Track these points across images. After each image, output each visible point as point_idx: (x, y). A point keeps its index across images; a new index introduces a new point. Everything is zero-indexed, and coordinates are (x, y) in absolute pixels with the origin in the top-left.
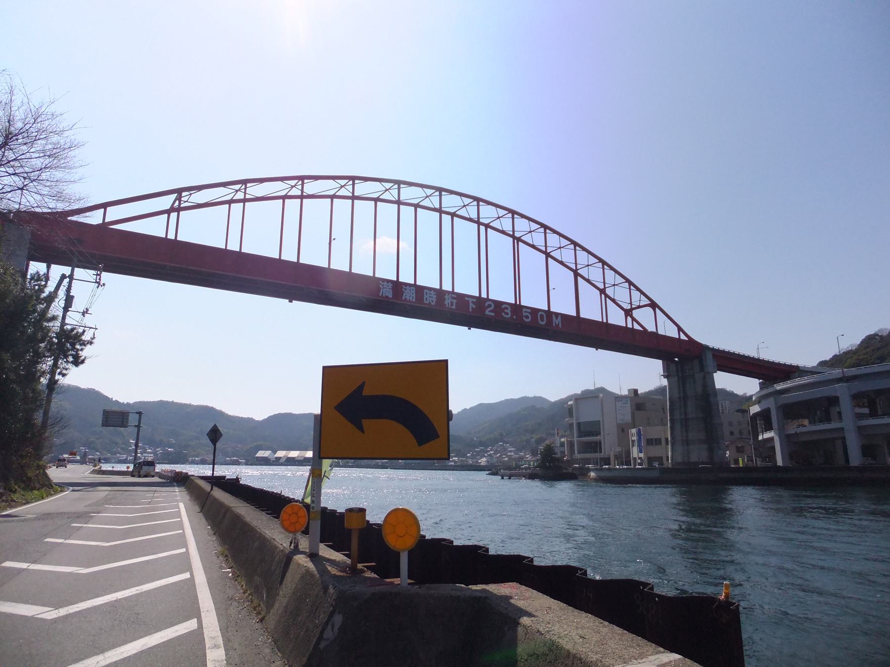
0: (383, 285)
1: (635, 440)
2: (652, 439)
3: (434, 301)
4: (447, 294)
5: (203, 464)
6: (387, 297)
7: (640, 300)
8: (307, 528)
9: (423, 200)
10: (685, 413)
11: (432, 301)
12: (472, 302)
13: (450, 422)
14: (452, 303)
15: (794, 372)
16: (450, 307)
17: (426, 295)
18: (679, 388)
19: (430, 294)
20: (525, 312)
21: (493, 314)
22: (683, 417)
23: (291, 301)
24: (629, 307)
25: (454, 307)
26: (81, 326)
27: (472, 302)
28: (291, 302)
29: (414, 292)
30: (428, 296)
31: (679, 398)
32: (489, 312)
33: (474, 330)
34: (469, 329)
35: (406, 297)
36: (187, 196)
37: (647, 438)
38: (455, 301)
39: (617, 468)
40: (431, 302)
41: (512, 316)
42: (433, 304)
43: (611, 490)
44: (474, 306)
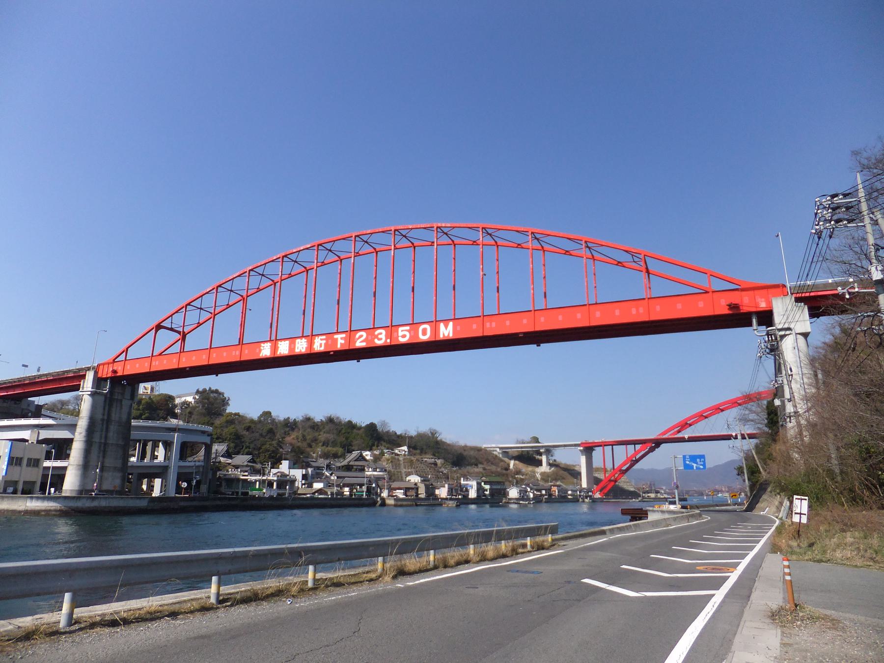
2: (32, 459)
6: (266, 355)
10: (106, 437)
11: (303, 348)
12: (341, 339)
18: (104, 409)
20: (402, 331)
21: (364, 344)
22: (103, 441)
23: (538, 345)
26: (801, 366)
27: (341, 339)
28: (539, 346)
31: (103, 420)
32: (361, 342)
33: (544, 346)
35: (281, 351)
39: (459, 498)
42: (451, 335)
44: (343, 342)
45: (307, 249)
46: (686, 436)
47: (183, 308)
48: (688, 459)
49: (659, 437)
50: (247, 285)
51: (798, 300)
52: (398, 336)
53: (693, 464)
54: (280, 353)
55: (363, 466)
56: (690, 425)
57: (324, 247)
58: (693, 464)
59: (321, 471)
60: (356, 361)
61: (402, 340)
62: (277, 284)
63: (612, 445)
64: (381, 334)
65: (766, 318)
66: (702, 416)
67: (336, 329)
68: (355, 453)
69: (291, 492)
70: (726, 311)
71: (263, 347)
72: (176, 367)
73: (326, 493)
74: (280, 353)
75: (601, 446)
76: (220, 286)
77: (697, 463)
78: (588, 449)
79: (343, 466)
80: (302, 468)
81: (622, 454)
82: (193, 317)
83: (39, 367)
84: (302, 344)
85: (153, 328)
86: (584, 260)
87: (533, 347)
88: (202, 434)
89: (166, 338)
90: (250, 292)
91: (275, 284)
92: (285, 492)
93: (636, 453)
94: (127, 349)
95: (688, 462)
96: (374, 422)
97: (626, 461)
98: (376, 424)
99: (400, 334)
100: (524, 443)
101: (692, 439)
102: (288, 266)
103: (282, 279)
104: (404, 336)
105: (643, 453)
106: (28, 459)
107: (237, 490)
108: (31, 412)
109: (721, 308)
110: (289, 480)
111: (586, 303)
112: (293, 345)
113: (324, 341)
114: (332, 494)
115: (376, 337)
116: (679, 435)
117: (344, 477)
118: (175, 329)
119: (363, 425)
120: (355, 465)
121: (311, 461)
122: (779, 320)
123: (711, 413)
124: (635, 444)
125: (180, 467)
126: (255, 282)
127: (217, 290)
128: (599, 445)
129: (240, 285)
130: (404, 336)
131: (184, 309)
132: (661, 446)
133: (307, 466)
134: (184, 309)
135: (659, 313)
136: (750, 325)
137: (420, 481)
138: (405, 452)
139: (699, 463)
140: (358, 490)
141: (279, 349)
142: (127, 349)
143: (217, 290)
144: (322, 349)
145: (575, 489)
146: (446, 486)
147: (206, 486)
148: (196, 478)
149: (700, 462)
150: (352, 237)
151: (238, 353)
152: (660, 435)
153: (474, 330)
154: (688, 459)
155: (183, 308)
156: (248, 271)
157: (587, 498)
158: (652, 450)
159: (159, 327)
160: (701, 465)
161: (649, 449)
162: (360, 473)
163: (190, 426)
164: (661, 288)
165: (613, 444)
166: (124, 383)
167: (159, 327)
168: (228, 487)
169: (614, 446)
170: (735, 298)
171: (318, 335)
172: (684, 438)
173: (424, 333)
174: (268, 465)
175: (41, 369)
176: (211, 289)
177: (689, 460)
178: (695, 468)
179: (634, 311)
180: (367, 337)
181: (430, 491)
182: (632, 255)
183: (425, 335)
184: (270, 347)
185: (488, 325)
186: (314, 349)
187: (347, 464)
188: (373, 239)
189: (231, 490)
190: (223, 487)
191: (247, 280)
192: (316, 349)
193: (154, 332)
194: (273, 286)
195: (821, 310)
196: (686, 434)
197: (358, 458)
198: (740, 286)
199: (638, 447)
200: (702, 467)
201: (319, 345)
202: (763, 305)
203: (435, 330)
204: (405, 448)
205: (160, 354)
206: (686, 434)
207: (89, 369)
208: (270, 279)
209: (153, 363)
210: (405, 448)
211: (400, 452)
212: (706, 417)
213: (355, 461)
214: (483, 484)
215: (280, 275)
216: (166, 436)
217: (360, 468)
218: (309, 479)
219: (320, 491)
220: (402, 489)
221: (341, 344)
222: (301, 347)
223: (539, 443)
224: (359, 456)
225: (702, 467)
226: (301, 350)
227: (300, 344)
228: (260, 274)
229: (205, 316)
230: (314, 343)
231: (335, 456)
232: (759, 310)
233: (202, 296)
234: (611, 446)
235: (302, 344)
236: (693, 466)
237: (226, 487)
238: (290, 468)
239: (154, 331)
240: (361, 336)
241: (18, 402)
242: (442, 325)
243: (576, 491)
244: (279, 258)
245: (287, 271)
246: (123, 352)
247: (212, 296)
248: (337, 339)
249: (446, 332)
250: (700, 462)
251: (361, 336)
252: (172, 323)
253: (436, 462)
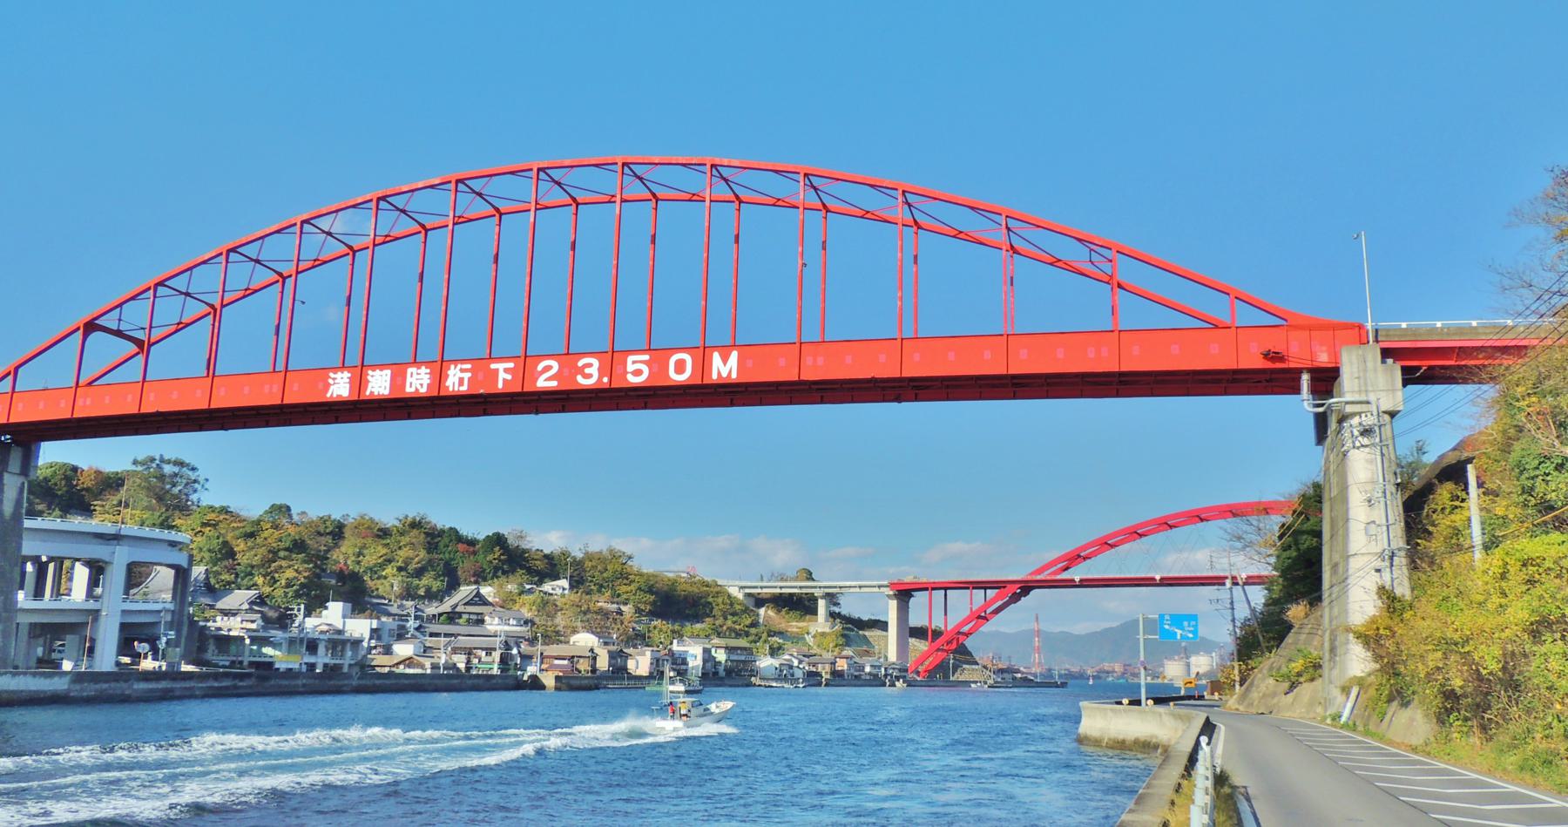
1: (432, 664)
5: (174, 542)
8: (1063, 718)
9: (788, 172)
11: (422, 385)
12: (506, 370)
14: (461, 381)
15: (1290, 596)
17: (412, 376)
19: (418, 374)
20: (634, 362)
21: (553, 384)
27: (506, 370)
32: (546, 380)
35: (373, 390)
42: (734, 376)
44: (509, 377)
45: (432, 187)
46: (1077, 579)
47: (149, 289)
48: (1167, 620)
49: (1030, 578)
50: (296, 252)
51: (1386, 353)
52: (626, 373)
53: (1176, 630)
54: (372, 393)
55: (482, 614)
56: (1085, 558)
57: (467, 186)
58: (1176, 630)
59: (404, 623)
61: (634, 380)
62: (287, 280)
63: (946, 589)
64: (590, 365)
65: (1326, 381)
66: (1105, 544)
67: (488, 351)
68: (465, 591)
69: (352, 662)
70: (1259, 363)
71: (334, 379)
72: (133, 410)
73: (422, 666)
74: (372, 393)
75: (926, 589)
76: (234, 250)
77: (1182, 629)
78: (904, 594)
79: (440, 615)
80: (371, 617)
81: (962, 605)
82: (169, 309)
84: (419, 377)
85: (78, 329)
86: (1004, 252)
88: (170, 548)
89: (103, 349)
90: (228, 297)
91: (284, 279)
92: (341, 662)
93: (988, 604)
94: (16, 369)
96: (501, 532)
97: (969, 617)
98: (506, 533)
99: (630, 368)
100: (786, 580)
101: (1086, 583)
102: (389, 221)
103: (376, 243)
104: (638, 373)
105: (999, 603)
107: (240, 659)
109: (1252, 359)
110: (349, 640)
111: (1002, 333)
112: (400, 379)
113: (469, 375)
114: (435, 667)
115: (581, 371)
116: (1065, 576)
117: (455, 635)
118: (127, 333)
119: (481, 537)
122: (1349, 387)
123: (1122, 539)
124: (985, 588)
125: (124, 612)
126: (241, 273)
127: (155, 292)
128: (923, 588)
129: (207, 282)
130: (637, 372)
131: (151, 291)
132: (1032, 593)
133: (378, 611)
134: (151, 291)
135: (1137, 360)
136: (1296, 390)
137: (596, 645)
138: (564, 589)
139: (1187, 629)
140: (483, 660)
141: (370, 385)
142: (16, 369)
143: (155, 292)
144: (464, 388)
145: (878, 664)
146: (648, 654)
147: (178, 649)
148: (166, 635)
149: (1189, 626)
150: (531, 170)
151: (277, 389)
152: (1032, 574)
153: (783, 371)
154: (1167, 620)
155: (149, 289)
156: (224, 254)
157: (898, 681)
158: (1015, 598)
159: (91, 327)
160: (1190, 632)
161: (1010, 598)
162: (477, 628)
164: (1136, 315)
165: (946, 588)
167: (91, 327)
168: (220, 652)
169: (948, 591)
170: (1275, 343)
171: (456, 362)
172: (1073, 580)
173: (680, 367)
174: (299, 610)
176: (214, 254)
177: (1169, 622)
178: (1179, 637)
179: (1091, 353)
180: (560, 371)
181: (619, 658)
183: (680, 371)
184: (348, 380)
185: (808, 361)
186: (448, 387)
187: (449, 610)
188: (570, 178)
189: (229, 658)
190: (210, 651)
191: (297, 242)
192: (451, 389)
193: (81, 337)
194: (279, 285)
195: (1418, 374)
196: (1076, 574)
197: (472, 599)
198: (1286, 320)
199: (991, 593)
200: (1191, 635)
201: (457, 380)
202: (1323, 359)
203: (703, 364)
204: (564, 583)
205: (90, 384)
206: (1076, 574)
208: (416, 221)
209: (79, 402)
210: (564, 583)
211: (553, 589)
212: (1112, 546)
213: (465, 604)
214: (713, 651)
215: (372, 236)
216: (98, 551)
217: (474, 617)
218: (385, 636)
219: (408, 662)
220: (565, 659)
221: (505, 381)
222: (418, 382)
223: (813, 580)
224: (475, 596)
225: (1191, 635)
226: (417, 389)
227: (415, 376)
228: (181, 293)
229: (194, 309)
230: (447, 376)
231: (431, 596)
232: (1316, 364)
233: (190, 269)
234: (943, 591)
235: (419, 377)
236: (1176, 633)
237: (216, 651)
238: (344, 617)
239: (79, 334)
240: (548, 368)
242: (716, 357)
243: (879, 667)
244: (371, 200)
245: (309, 254)
246: (9, 374)
247: (291, 240)
248: (497, 371)
249: (725, 368)
250: (1189, 626)
251: (548, 368)
252: (120, 320)
253: (620, 609)
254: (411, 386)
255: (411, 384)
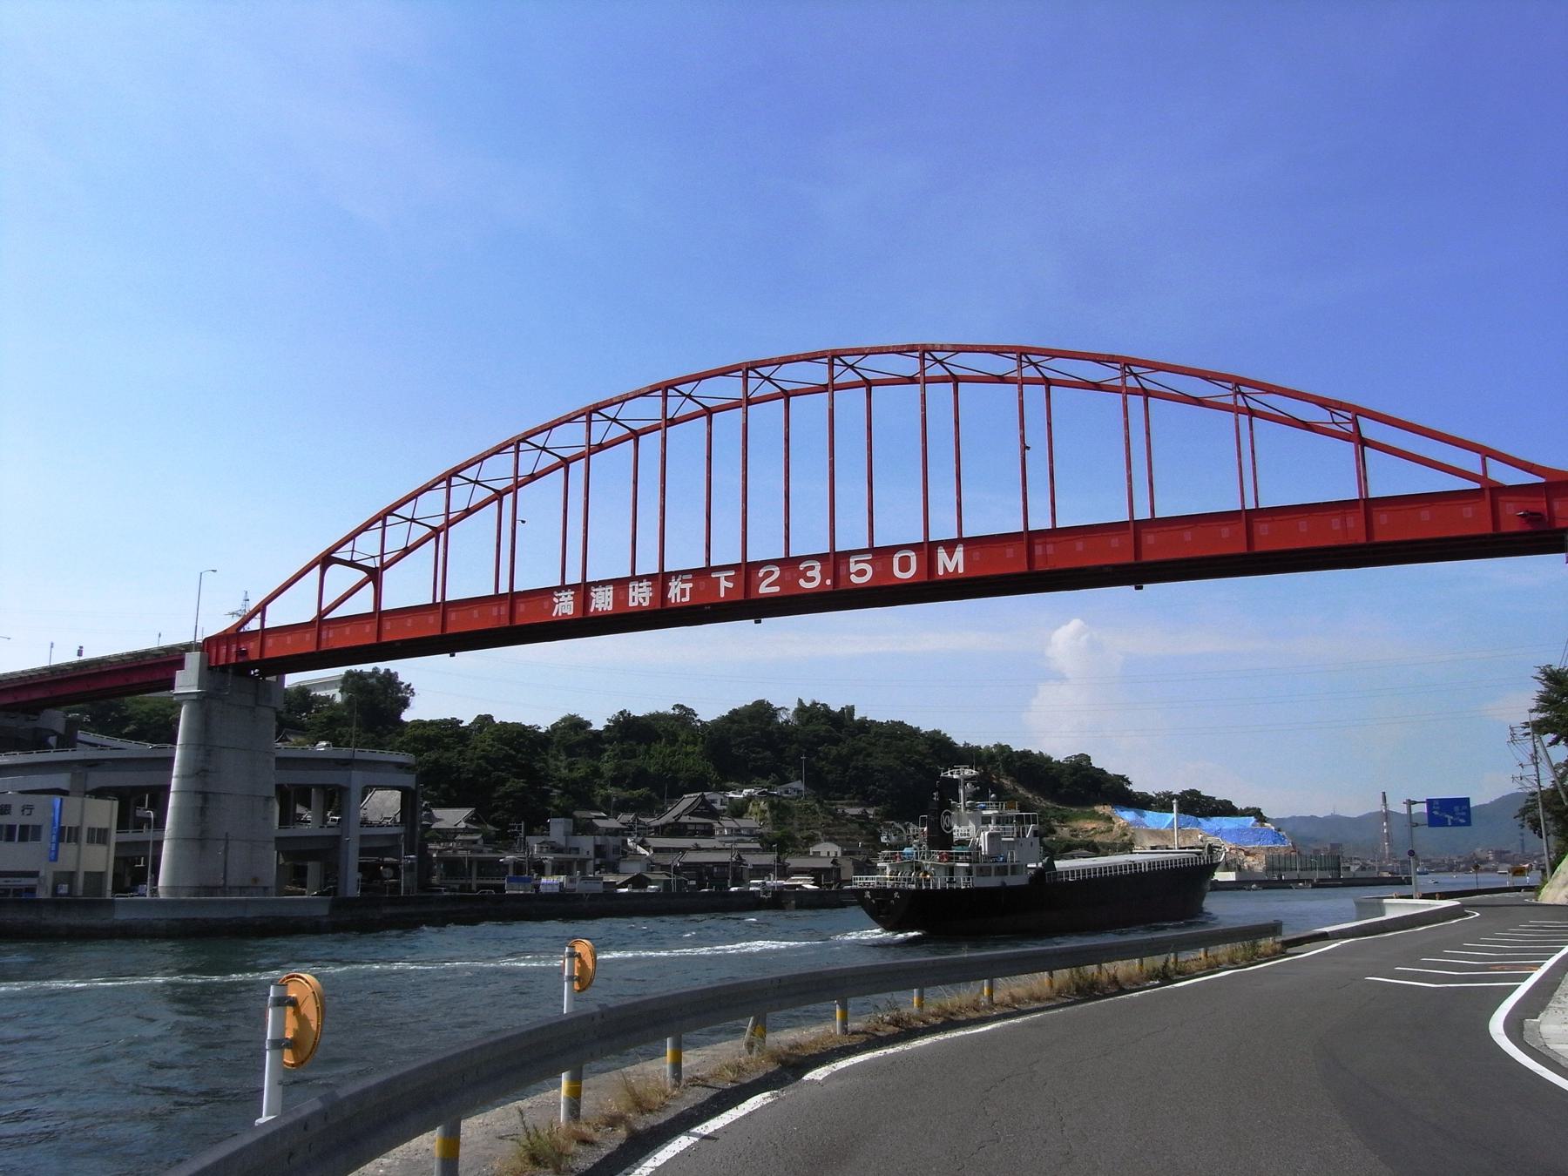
0: (559, 597)
3: (647, 599)
4: (673, 577)
7: (353, 551)
11: (644, 598)
12: (727, 578)
13: (1135, 788)
14: (683, 592)
16: (678, 601)
21: (776, 589)
24: (377, 563)
25: (687, 599)
28: (1141, 588)
29: (611, 593)
30: (635, 594)
32: (768, 586)
34: (1137, 588)
36: (1345, 417)
37: (38, 887)
38: (688, 586)
40: (642, 601)
41: (823, 581)
43: (1316, 890)
44: (730, 585)
53: (1447, 816)
54: (596, 609)
58: (1447, 816)
60: (753, 621)
74: (596, 609)
79: (664, 826)
83: (81, 647)
87: (1129, 590)
89: (340, 578)
95: (1436, 813)
99: (854, 568)
104: (861, 573)
106: (89, 829)
108: (55, 733)
113: (691, 585)
115: (803, 575)
120: (691, 823)
121: (597, 818)
160: (1461, 817)
163: (344, 753)
166: (255, 673)
174: (520, 828)
175: (1386, 794)
177: (1438, 808)
182: (1332, 412)
207: (188, 648)
235: (641, 590)
241: (32, 717)
247: (439, 494)
254: (634, 601)
255: (634, 597)
